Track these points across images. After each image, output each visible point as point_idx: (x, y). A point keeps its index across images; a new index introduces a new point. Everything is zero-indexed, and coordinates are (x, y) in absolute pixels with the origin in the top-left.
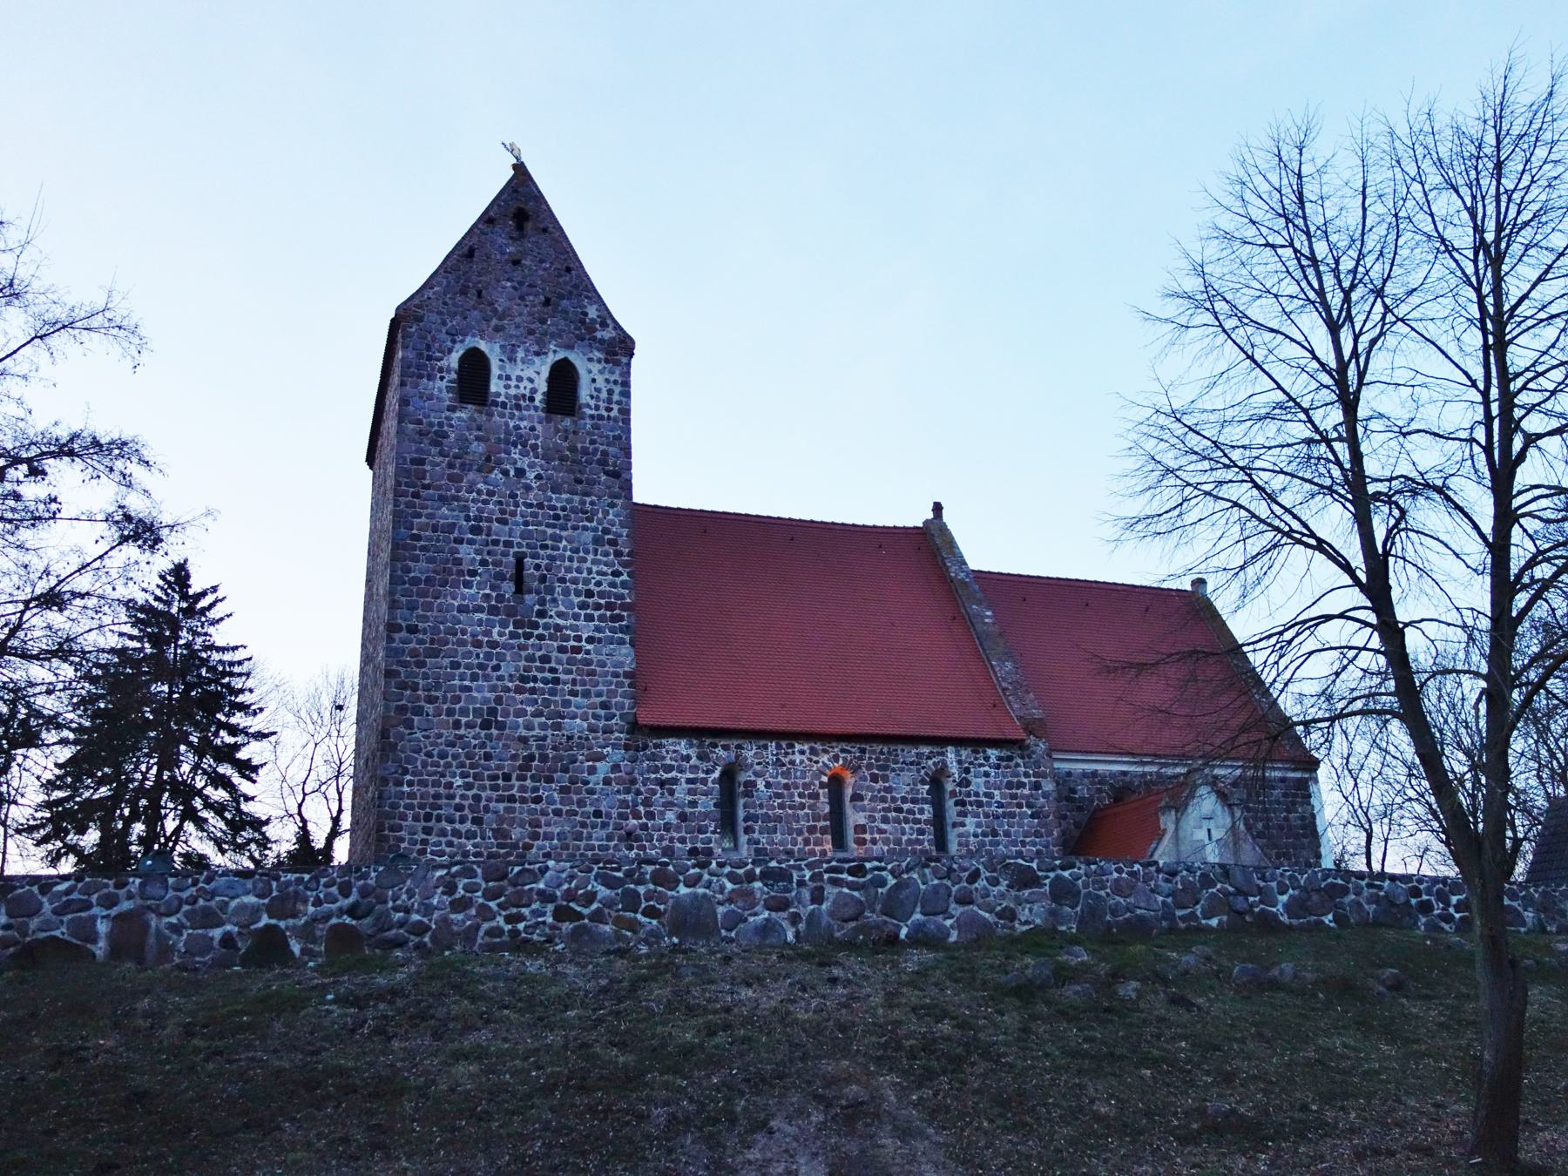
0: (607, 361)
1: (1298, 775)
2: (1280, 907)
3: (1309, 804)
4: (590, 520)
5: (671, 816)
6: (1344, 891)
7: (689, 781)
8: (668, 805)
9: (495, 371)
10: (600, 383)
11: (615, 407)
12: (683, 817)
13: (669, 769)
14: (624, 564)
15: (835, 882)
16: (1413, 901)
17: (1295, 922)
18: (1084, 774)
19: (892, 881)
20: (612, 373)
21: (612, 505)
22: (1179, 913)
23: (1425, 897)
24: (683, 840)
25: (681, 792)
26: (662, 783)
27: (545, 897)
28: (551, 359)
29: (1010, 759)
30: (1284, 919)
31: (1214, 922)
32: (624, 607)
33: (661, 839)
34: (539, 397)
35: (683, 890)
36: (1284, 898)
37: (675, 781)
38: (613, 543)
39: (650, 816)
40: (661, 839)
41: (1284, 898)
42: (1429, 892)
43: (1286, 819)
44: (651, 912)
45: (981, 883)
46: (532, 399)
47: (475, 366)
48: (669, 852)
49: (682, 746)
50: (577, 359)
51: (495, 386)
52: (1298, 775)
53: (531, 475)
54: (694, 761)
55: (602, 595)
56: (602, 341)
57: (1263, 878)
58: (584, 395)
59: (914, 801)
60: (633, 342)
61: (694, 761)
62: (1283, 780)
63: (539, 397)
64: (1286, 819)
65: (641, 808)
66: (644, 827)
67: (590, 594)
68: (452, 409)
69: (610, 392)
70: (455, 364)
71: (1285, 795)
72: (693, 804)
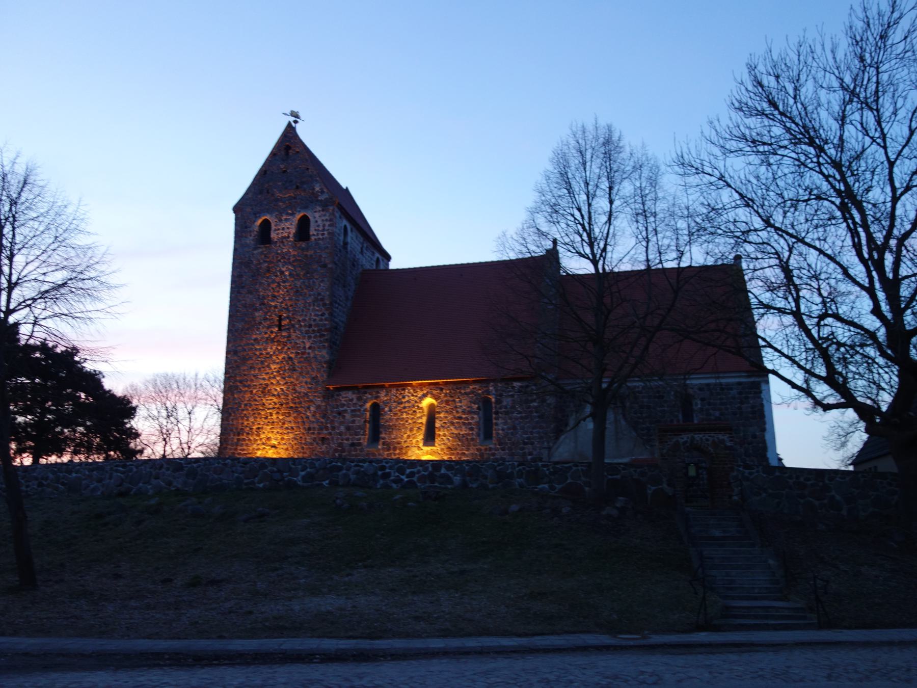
0: (323, 210)
1: (752, 379)
2: (300, 478)
3: (760, 397)
4: (312, 290)
5: (342, 428)
6: (340, 469)
7: (352, 411)
8: (341, 423)
9: (273, 227)
10: (320, 222)
11: (326, 232)
12: (348, 428)
13: (343, 405)
14: (326, 310)
15: (117, 471)
16: (380, 473)
17: (305, 484)
18: (716, 384)
19: (135, 470)
20: (325, 215)
21: (322, 281)
22: (246, 481)
23: (387, 471)
24: (347, 439)
25: (348, 416)
26: (339, 413)
27: (36, 478)
28: (298, 216)
29: (527, 386)
30: (300, 483)
31: (261, 485)
32: (326, 330)
33: (338, 439)
34: (291, 236)
35: (74, 475)
36: (303, 473)
37: (346, 411)
38: (322, 300)
39: (333, 428)
40: (338, 439)
41: (303, 473)
42: (390, 468)
43: (740, 408)
44: (63, 484)
45: (163, 470)
46: (288, 237)
47: (266, 225)
48: (340, 445)
49: (350, 395)
50: (309, 214)
51: (273, 235)
52: (752, 379)
53: (287, 273)
54: (355, 401)
55: (317, 325)
56: (321, 201)
57: (294, 464)
58: (312, 231)
59: (469, 413)
60: (237, 209)
61: (355, 401)
62: (739, 384)
63: (291, 236)
64: (740, 408)
65: (329, 425)
66: (330, 434)
67: (310, 326)
68: (255, 249)
69: (324, 226)
70: (256, 229)
71: (740, 393)
72: (353, 422)
